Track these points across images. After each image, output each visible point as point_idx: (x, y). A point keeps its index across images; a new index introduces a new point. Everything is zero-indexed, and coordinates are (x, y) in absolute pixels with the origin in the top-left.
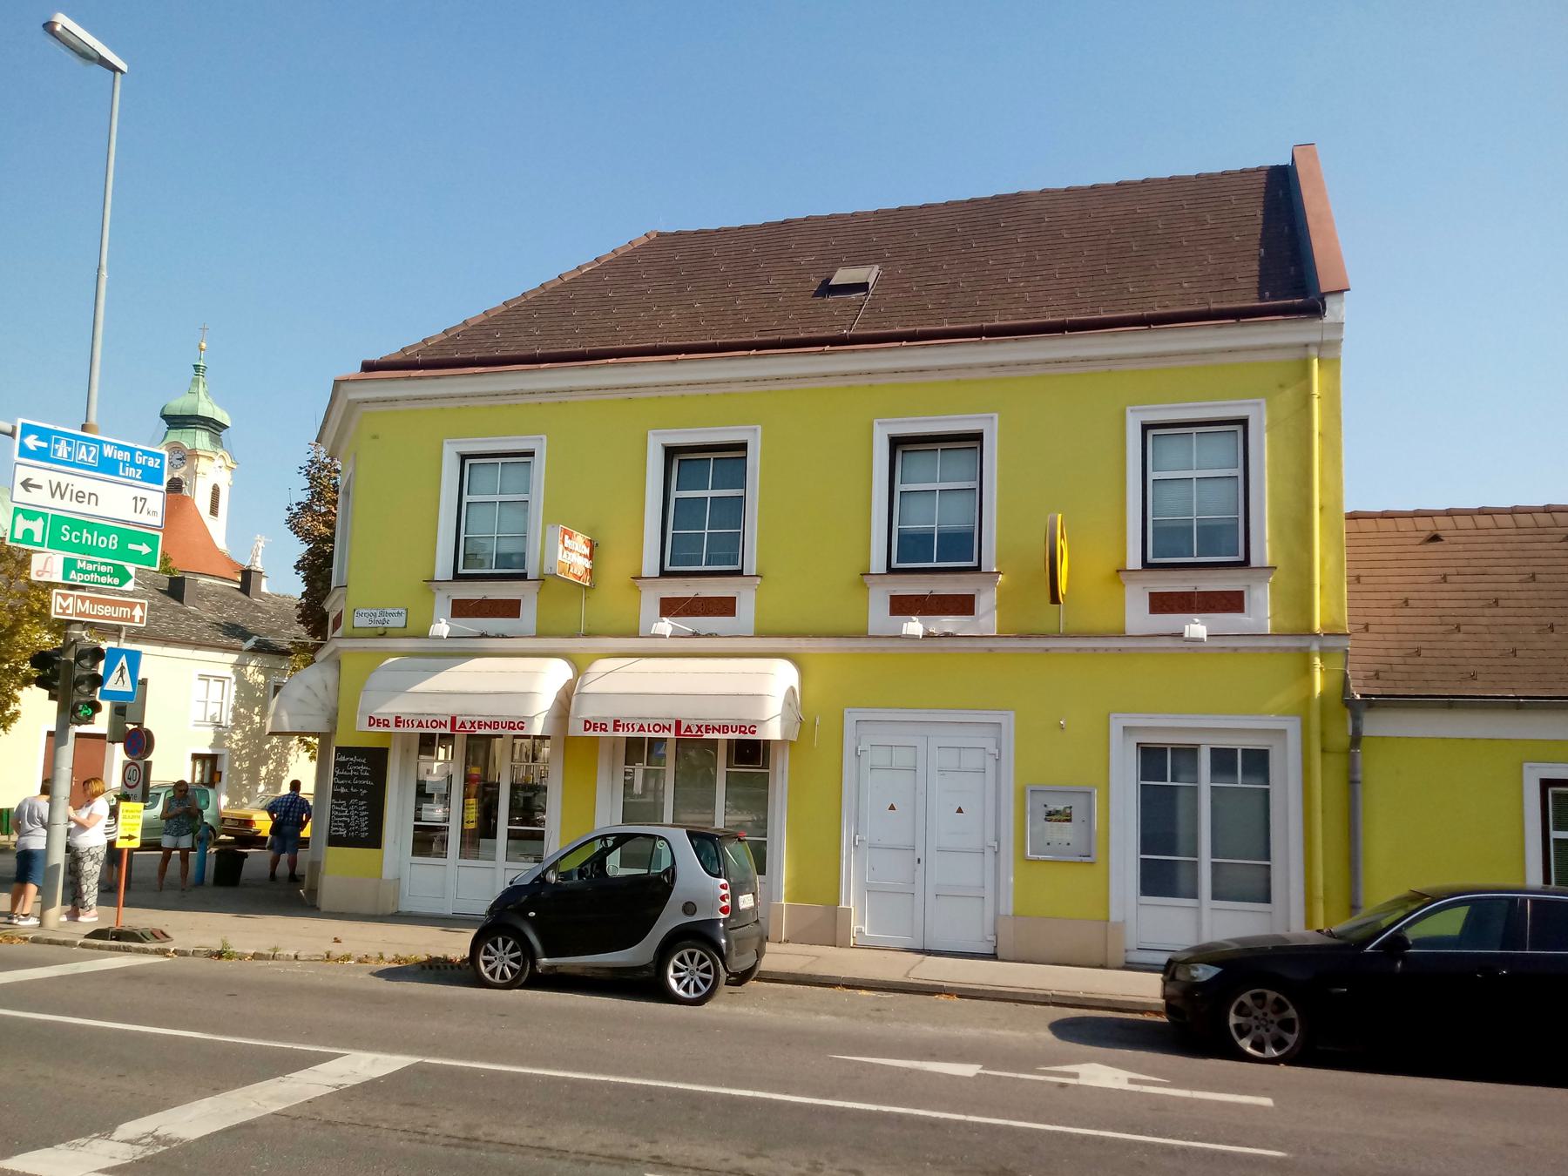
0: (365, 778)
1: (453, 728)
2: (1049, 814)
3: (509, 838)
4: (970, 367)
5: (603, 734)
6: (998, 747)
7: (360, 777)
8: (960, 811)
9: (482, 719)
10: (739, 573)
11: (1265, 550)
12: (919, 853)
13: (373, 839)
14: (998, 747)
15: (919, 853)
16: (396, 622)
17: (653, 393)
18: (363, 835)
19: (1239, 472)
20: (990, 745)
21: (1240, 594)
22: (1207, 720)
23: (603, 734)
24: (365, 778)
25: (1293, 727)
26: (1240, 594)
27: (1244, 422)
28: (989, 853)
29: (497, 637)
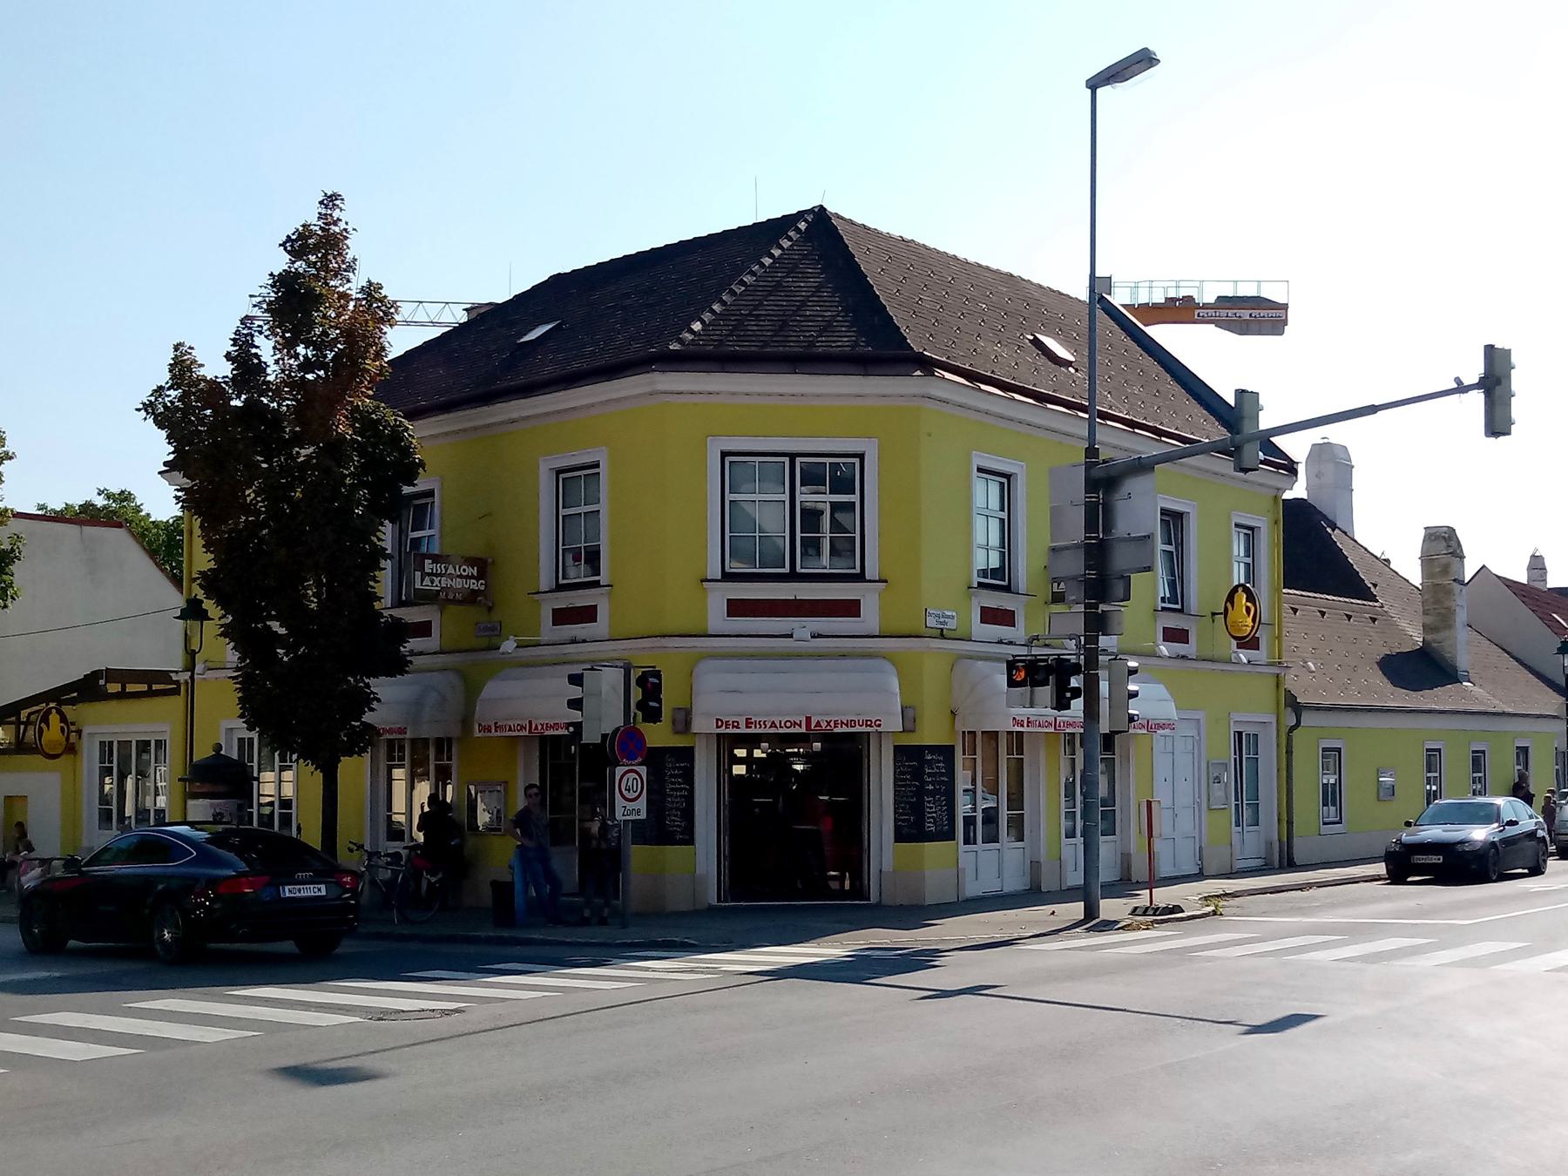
20: (1194, 733)
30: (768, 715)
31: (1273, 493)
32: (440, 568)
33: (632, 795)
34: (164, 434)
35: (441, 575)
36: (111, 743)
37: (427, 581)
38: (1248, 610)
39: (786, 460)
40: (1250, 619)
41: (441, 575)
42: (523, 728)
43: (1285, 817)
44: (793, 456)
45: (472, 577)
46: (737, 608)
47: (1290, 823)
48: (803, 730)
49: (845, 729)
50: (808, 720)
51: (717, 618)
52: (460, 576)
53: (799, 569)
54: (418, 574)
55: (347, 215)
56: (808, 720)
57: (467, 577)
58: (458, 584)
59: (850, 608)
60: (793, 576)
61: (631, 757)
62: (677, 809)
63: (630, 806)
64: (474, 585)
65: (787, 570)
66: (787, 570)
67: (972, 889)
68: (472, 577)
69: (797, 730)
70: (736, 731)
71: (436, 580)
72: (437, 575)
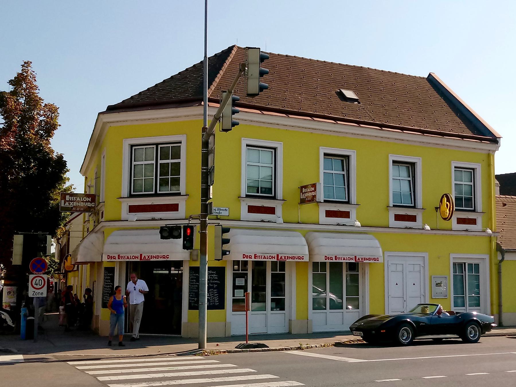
0: (216, 280)
1: (278, 259)
2: (437, 284)
3: (272, 301)
4: (415, 142)
5: (114, 260)
6: (424, 264)
7: (214, 280)
8: (397, 284)
9: (289, 256)
10: (179, 194)
11: (480, 207)
12: (405, 299)
13: (221, 306)
14: (424, 264)
15: (405, 299)
16: (224, 213)
17: (258, 124)
18: (216, 304)
19: (273, 166)
20: (421, 263)
21: (177, 205)
22: (468, 257)
23: (114, 260)
24: (216, 280)
25: (487, 257)
26: (177, 205)
27: (275, 149)
28: (422, 297)
29: (269, 222)
30: (126, 253)
31: (487, 152)
32: (72, 198)
33: (38, 287)
34: (64, 159)
35: (74, 201)
36: (465, 263)
37: (67, 203)
38: (447, 205)
39: (155, 146)
40: (448, 210)
41: (74, 201)
42: (136, 257)
43: (495, 302)
44: (157, 145)
45: (89, 201)
46: (133, 209)
47: (500, 306)
48: (354, 261)
49: (155, 260)
50: (356, 257)
51: (124, 213)
52: (83, 201)
53: (158, 192)
54: (63, 201)
55: (33, 68)
56: (141, 255)
57: (86, 202)
58: (82, 204)
59: (174, 208)
60: (156, 195)
61: (39, 271)
62: (108, 293)
63: (36, 291)
64: (89, 204)
65: (154, 192)
66: (154, 192)
67: (317, 329)
68: (89, 201)
69: (137, 260)
70: (332, 261)
71: (71, 203)
72: (72, 201)
